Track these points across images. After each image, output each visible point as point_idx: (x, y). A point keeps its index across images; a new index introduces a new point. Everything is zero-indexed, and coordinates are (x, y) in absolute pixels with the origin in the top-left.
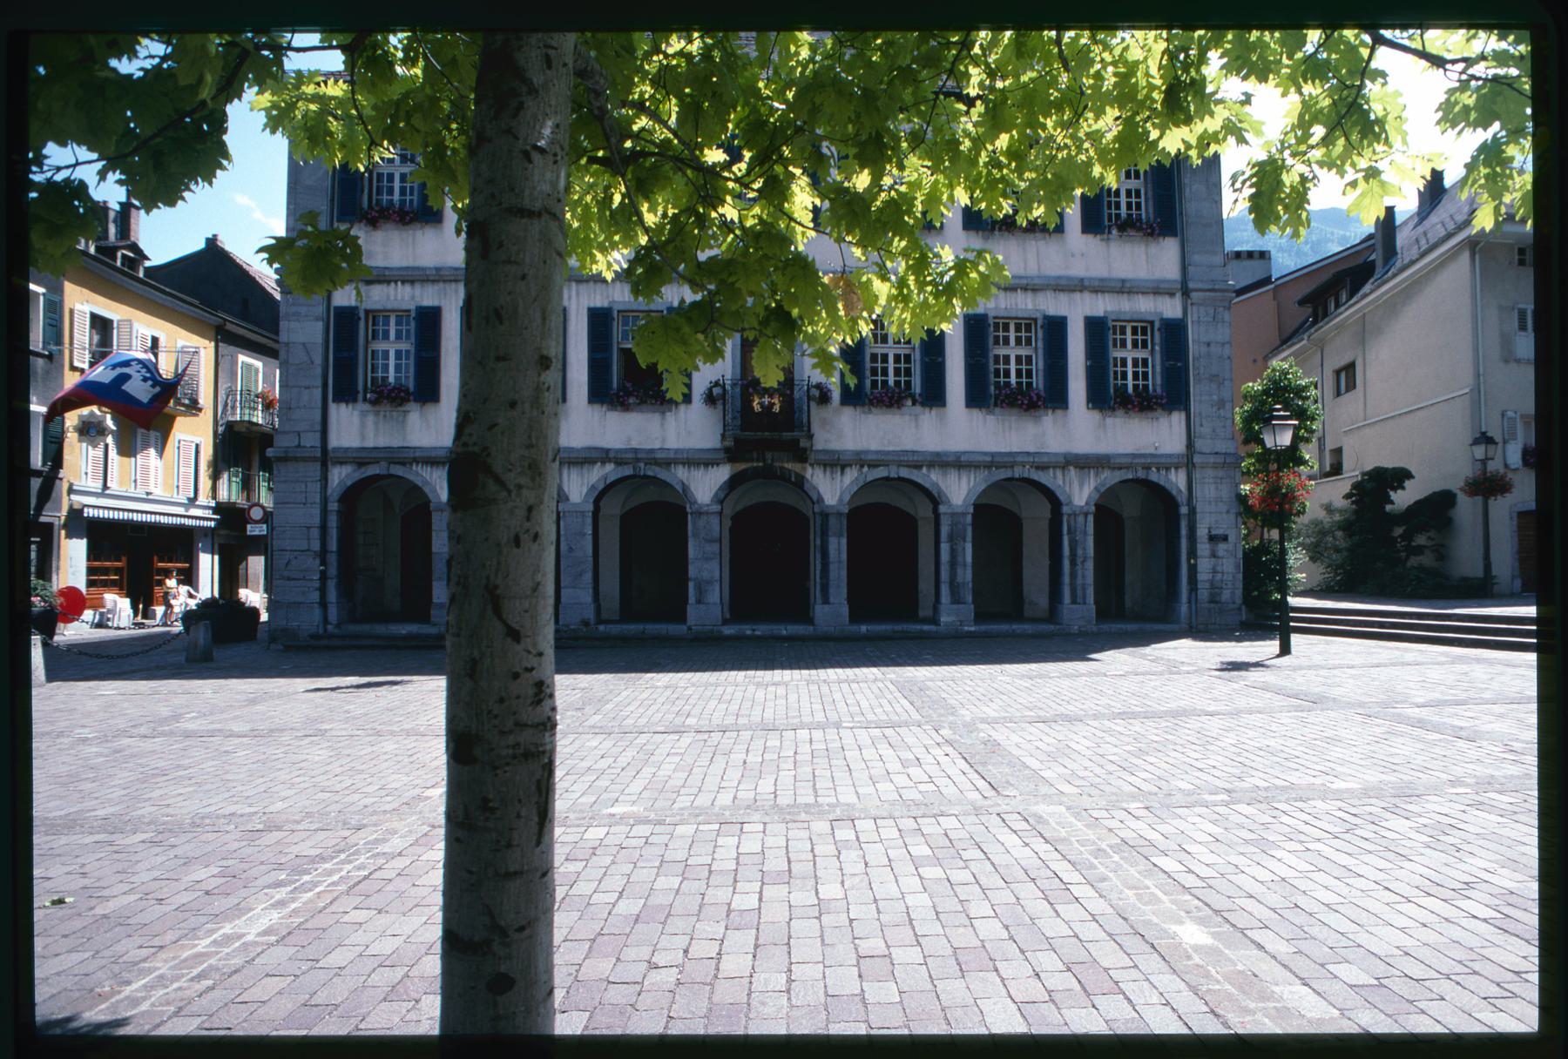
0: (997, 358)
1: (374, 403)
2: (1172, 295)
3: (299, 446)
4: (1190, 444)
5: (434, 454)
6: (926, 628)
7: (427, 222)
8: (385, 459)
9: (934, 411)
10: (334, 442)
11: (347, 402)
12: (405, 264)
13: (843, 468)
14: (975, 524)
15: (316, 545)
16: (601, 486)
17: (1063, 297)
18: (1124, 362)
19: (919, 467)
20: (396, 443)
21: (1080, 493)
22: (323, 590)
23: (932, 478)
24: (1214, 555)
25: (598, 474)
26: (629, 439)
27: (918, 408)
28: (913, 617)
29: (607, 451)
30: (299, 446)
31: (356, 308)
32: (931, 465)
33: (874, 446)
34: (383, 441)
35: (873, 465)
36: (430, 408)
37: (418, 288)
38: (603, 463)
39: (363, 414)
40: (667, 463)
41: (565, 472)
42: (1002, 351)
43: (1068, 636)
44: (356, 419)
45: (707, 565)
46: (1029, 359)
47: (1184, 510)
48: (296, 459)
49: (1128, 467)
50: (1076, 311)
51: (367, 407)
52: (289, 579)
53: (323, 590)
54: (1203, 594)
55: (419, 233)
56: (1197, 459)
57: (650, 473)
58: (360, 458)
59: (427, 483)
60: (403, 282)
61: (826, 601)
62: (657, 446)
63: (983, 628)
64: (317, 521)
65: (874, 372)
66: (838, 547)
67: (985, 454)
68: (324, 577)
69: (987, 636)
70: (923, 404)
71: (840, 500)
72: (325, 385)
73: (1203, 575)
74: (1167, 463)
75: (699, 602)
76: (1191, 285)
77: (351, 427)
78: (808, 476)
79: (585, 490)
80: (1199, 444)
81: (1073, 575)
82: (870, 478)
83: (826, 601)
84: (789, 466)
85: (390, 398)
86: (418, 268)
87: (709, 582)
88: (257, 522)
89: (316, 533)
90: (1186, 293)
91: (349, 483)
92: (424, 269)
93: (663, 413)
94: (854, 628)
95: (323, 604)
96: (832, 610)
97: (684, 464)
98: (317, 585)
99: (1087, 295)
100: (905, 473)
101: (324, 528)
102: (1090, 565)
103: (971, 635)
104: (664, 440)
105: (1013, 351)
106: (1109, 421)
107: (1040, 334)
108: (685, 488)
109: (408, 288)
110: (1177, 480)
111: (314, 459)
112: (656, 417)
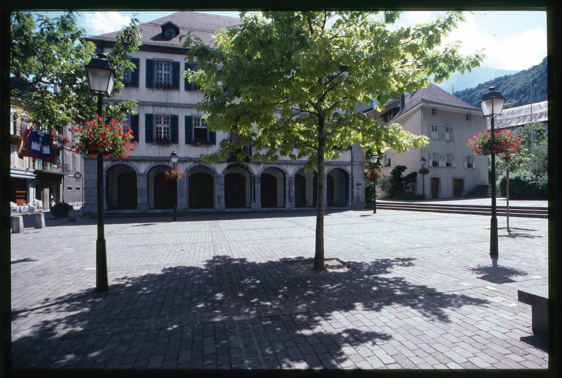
4: (352, 159)
13: (259, 164)
14: (295, 180)
23: (134, 165)
24: (358, 189)
29: (191, 158)
31: (152, 115)
32: (284, 164)
47: (350, 177)
49: (336, 165)
54: (355, 199)
55: (131, 90)
61: (254, 202)
73: (355, 194)
74: (346, 164)
75: (218, 202)
80: (354, 159)
83: (254, 202)
87: (221, 197)
94: (262, 209)
103: (294, 211)
108: (214, 170)
110: (349, 169)
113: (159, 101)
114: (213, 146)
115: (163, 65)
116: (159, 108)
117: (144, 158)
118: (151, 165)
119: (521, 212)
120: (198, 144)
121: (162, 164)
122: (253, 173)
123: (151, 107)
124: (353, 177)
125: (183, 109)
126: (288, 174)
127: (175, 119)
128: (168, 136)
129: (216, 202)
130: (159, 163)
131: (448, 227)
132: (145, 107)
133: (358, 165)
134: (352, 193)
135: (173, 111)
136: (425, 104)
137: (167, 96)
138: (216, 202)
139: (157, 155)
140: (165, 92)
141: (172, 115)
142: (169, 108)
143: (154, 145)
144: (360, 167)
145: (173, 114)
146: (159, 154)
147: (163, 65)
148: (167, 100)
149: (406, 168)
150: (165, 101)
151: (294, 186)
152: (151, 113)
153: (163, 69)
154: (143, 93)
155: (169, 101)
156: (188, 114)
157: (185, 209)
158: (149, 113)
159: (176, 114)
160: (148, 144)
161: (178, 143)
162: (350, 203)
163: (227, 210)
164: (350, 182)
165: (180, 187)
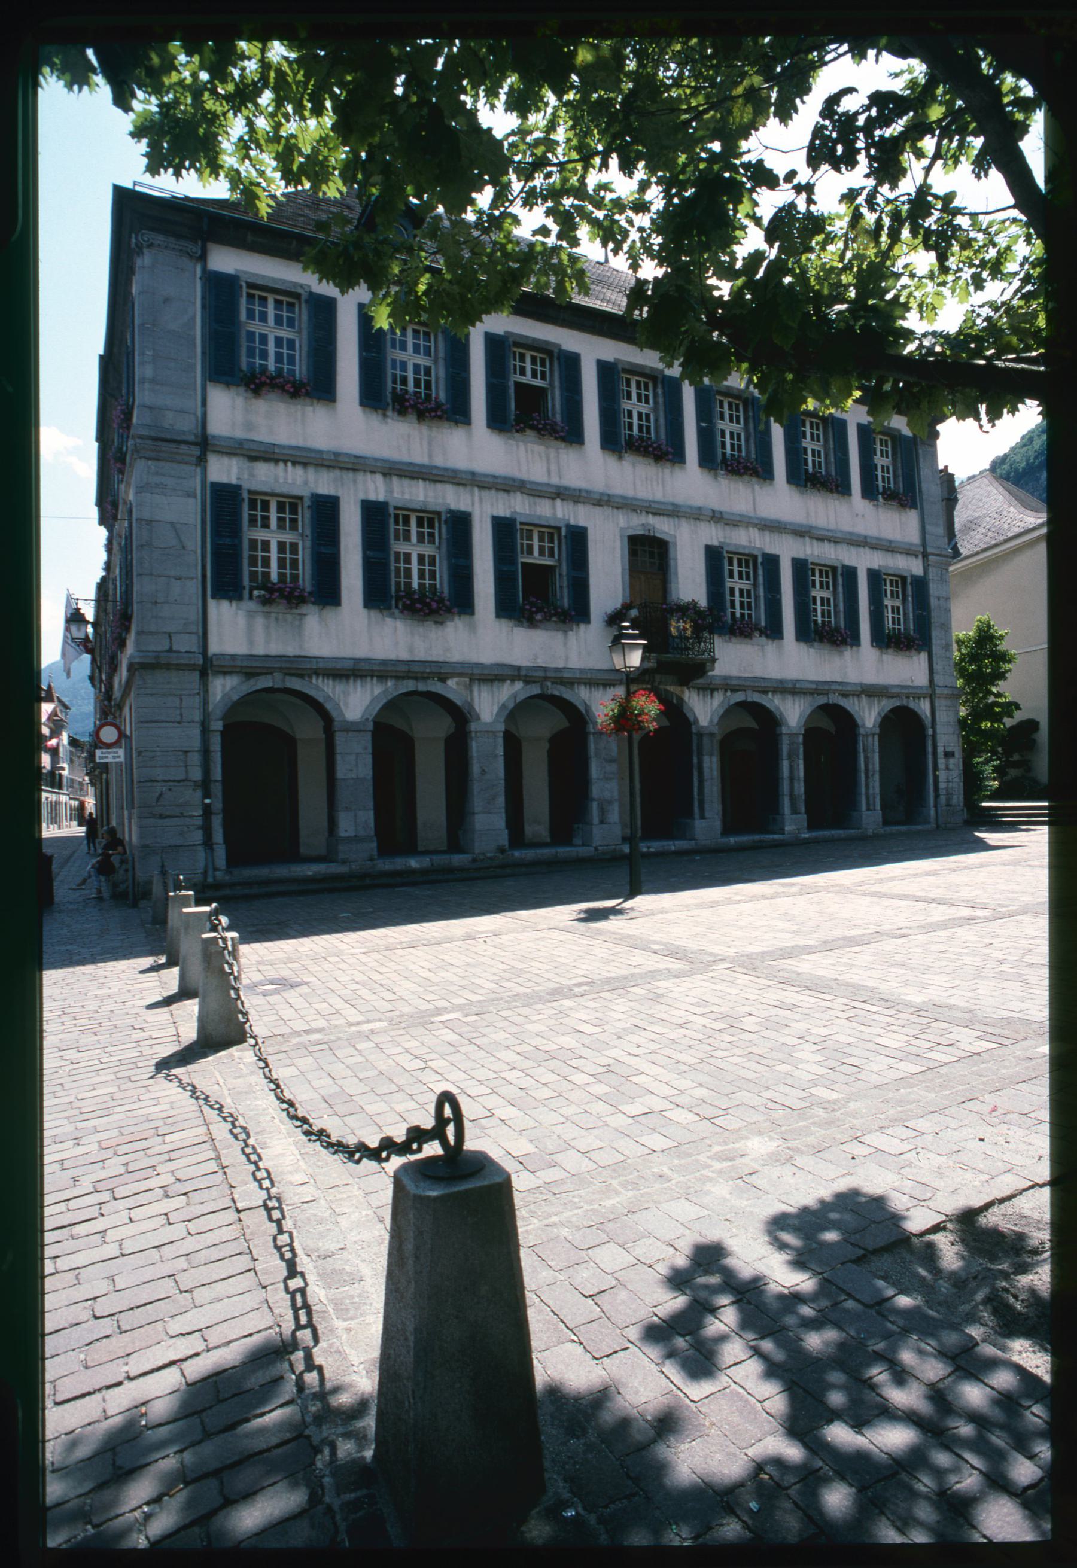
0: (253, 543)
1: (265, 602)
2: (916, 556)
3: (170, 650)
4: (931, 680)
5: (339, 666)
6: (776, 837)
7: (319, 399)
8: (280, 669)
9: (234, 604)
10: (214, 648)
11: (230, 599)
12: (293, 443)
13: (712, 691)
14: (805, 744)
15: (197, 774)
16: (511, 705)
17: (853, 550)
18: (408, 558)
19: (765, 692)
20: (291, 651)
21: (488, 706)
22: (207, 829)
23: (325, 689)
24: (947, 768)
25: (509, 692)
26: (536, 657)
27: (764, 639)
28: (294, 856)
29: (519, 668)
30: (170, 650)
31: (238, 487)
32: (775, 691)
33: (734, 673)
34: (276, 648)
35: (734, 690)
36: (330, 613)
37: (311, 473)
38: (513, 681)
39: (250, 615)
40: (571, 683)
41: (476, 689)
42: (261, 535)
43: (863, 838)
44: (242, 621)
45: (608, 783)
46: (294, 547)
47: (930, 732)
48: (168, 667)
49: (898, 696)
50: (352, 496)
51: (252, 605)
52: (162, 817)
53: (207, 829)
54: (943, 799)
55: (309, 409)
56: (938, 691)
57: (557, 693)
58: (248, 667)
59: (328, 698)
60: (294, 463)
61: (702, 817)
62: (561, 665)
63: (815, 834)
64: (197, 743)
65: (253, 561)
66: (711, 765)
67: (812, 682)
68: (207, 811)
69: (816, 841)
70: (767, 637)
71: (711, 721)
72: (204, 576)
73: (942, 785)
74: (916, 694)
75: (602, 822)
76: (929, 550)
77: (235, 629)
78: (686, 699)
79: (496, 709)
80: (938, 679)
81: (867, 786)
82: (732, 702)
83: (702, 817)
84: (671, 688)
85: (284, 596)
86: (309, 450)
87: (610, 802)
88: (109, 746)
89: (195, 759)
90: (925, 555)
91: (235, 697)
92: (320, 452)
93: (565, 632)
94: (725, 840)
95: (208, 843)
96: (793, 823)
97: (585, 684)
98: (199, 822)
99: (867, 550)
100: (756, 697)
101: (206, 752)
102: (877, 777)
103: (806, 842)
104: (567, 659)
105: (273, 537)
106: (885, 657)
107: (308, 515)
108: (588, 708)
109: (299, 471)
110: (924, 707)
111: (191, 667)
112: (559, 635)
113: (406, 459)
114: (582, 626)
115: (528, 360)
116: (406, 482)
117: (416, 668)
118: (386, 691)
120: (539, 617)
121: (422, 687)
122: (696, 721)
123: (379, 478)
125: (486, 494)
126: (478, 718)
127: (326, 510)
128: (295, 577)
130: (410, 685)
132: (360, 476)
133: (947, 697)
135: (453, 499)
137: (430, 444)
138: (864, 807)
139: (405, 656)
140: (425, 429)
141: (450, 511)
142: (439, 486)
143: (392, 616)
145: (453, 507)
146: (411, 649)
147: (528, 360)
148: (430, 456)
149: (1018, 707)
150: (425, 461)
151: (801, 762)
152: (381, 498)
153: (634, 396)
154: (345, 424)
155: (439, 461)
156: (502, 511)
157: (502, 850)
158: (372, 497)
159: (463, 507)
160: (375, 614)
161: (782, 638)
163: (386, 865)
164: (930, 749)
165: (483, 772)
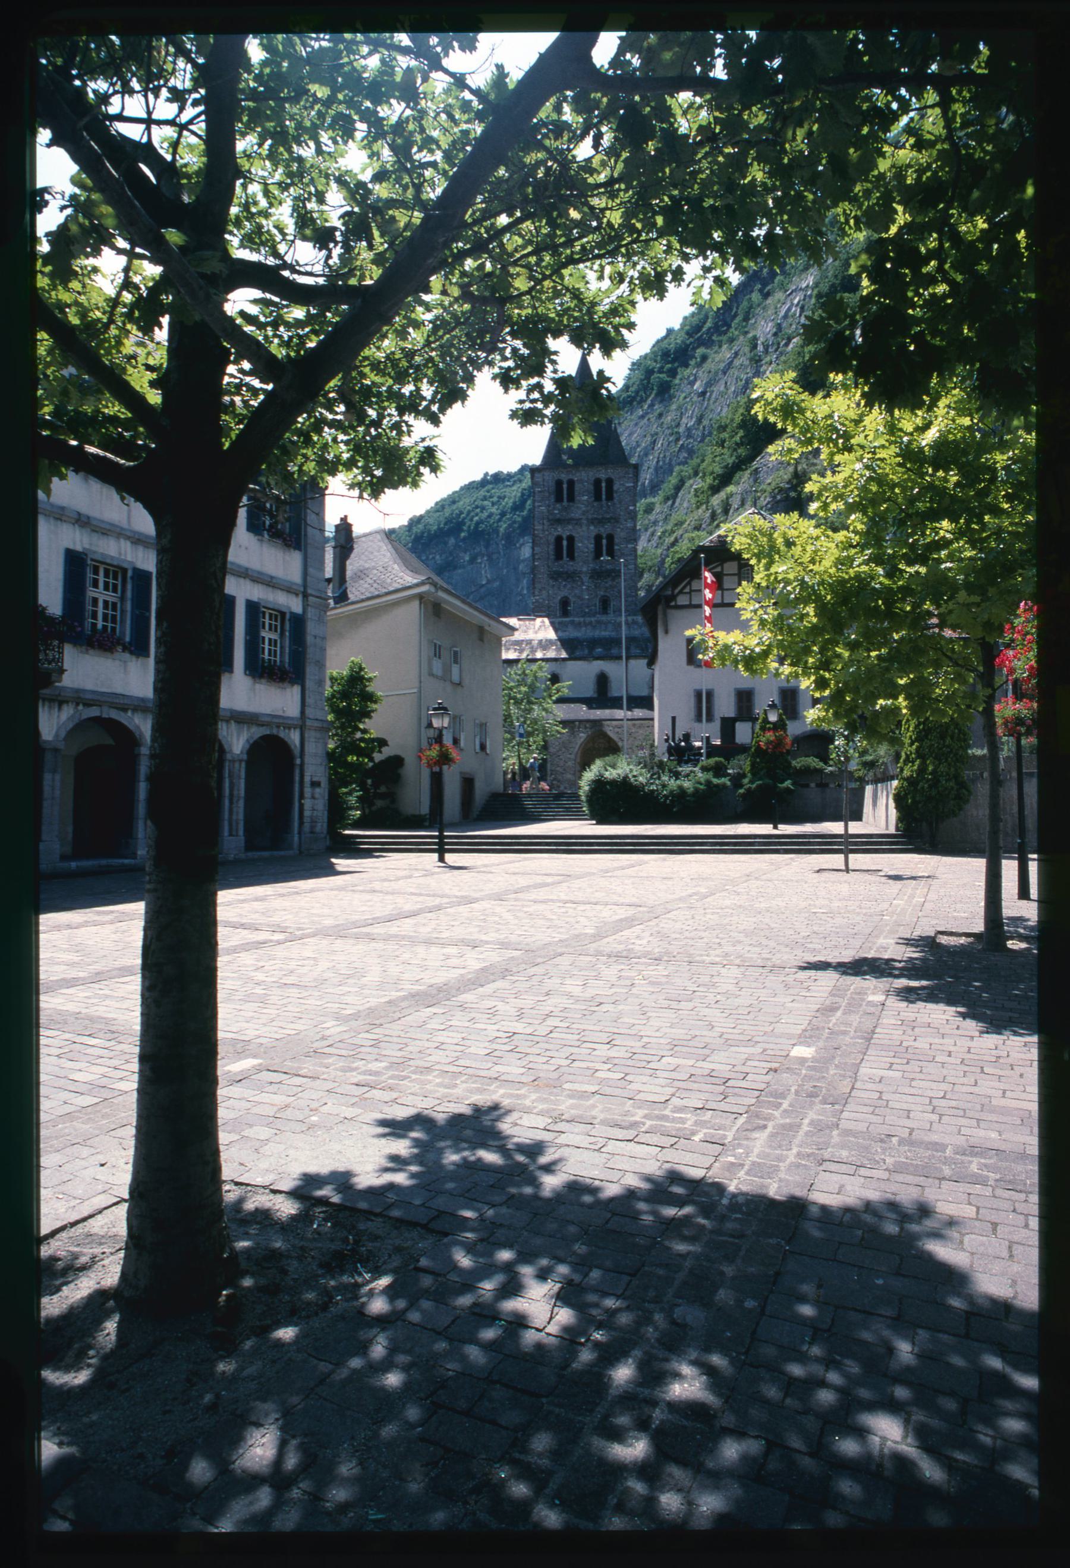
4: (303, 712)
24: (313, 797)
47: (298, 761)
54: (307, 827)
73: (307, 813)
74: (286, 723)
75: (231, 835)
119: (735, 844)
124: (302, 765)
126: (231, 751)
129: (226, 833)
130: (94, 712)
131: (376, 921)
134: (301, 806)
136: (433, 590)
138: (226, 833)
144: (318, 735)
162: (296, 838)
164: (297, 778)
